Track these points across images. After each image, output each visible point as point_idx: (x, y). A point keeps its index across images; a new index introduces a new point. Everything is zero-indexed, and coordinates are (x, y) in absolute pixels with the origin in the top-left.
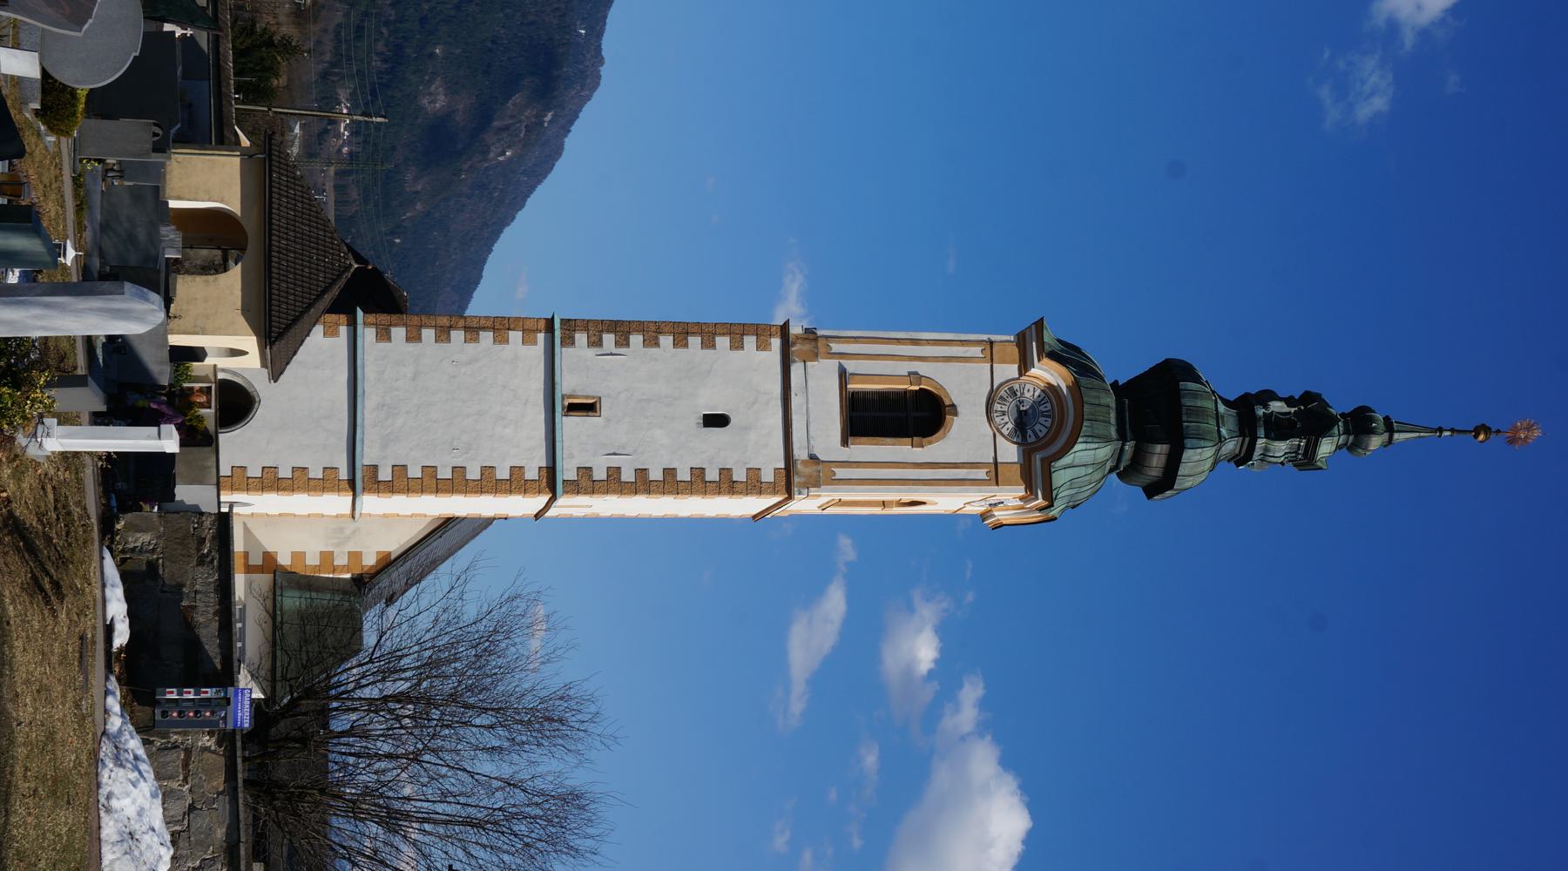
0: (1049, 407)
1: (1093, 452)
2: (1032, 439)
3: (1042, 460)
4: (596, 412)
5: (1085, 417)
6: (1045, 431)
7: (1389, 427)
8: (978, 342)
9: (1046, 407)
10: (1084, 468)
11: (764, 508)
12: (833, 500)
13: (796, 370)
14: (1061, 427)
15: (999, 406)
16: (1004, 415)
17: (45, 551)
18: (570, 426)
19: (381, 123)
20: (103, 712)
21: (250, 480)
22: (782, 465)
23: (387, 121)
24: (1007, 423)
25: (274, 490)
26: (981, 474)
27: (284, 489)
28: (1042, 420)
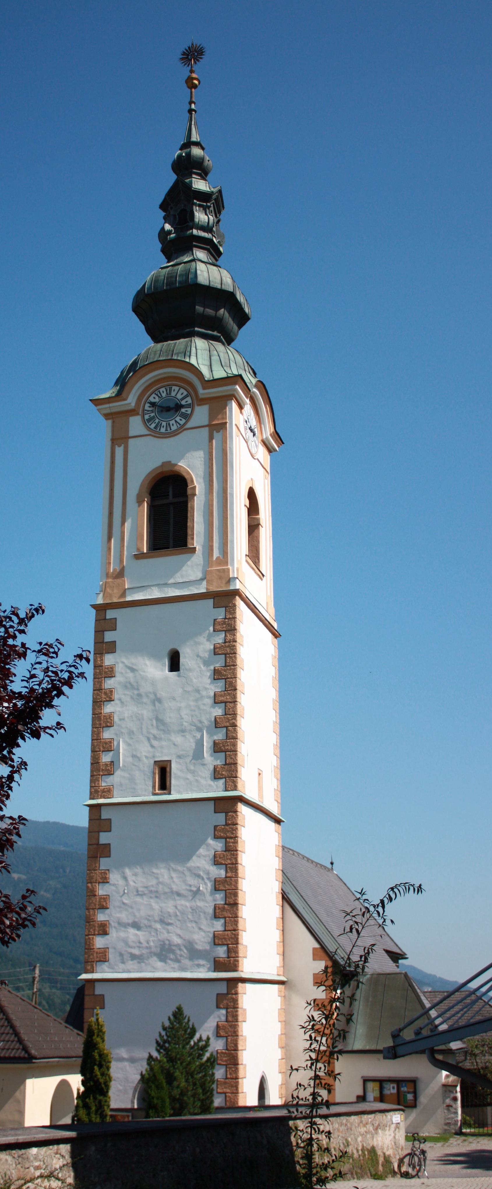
0: (163, 389)
1: (199, 352)
2: (189, 400)
3: (204, 388)
4: (167, 765)
5: (169, 358)
6: (182, 390)
7: (188, 144)
9: (163, 392)
10: (212, 358)
11: (261, 624)
12: (247, 561)
15: (162, 428)
16: (169, 424)
19: (40, 971)
21: (229, 1076)
22: (211, 602)
23: (38, 965)
24: (176, 421)
25: (237, 1054)
27: (236, 1045)
28: (173, 394)
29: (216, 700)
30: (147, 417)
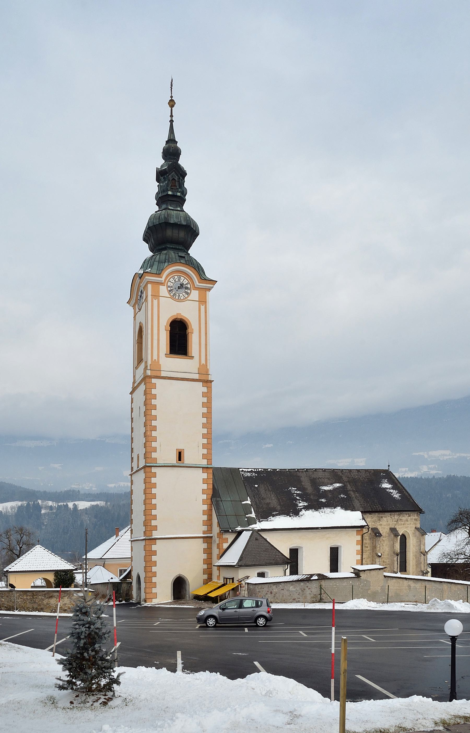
8: (152, 302)
13: (163, 374)
14: (182, 272)
17: (450, 495)
18: (187, 459)
20: (308, 584)
26: (203, 307)
28: (181, 281)
29: (204, 446)
30: (169, 289)
